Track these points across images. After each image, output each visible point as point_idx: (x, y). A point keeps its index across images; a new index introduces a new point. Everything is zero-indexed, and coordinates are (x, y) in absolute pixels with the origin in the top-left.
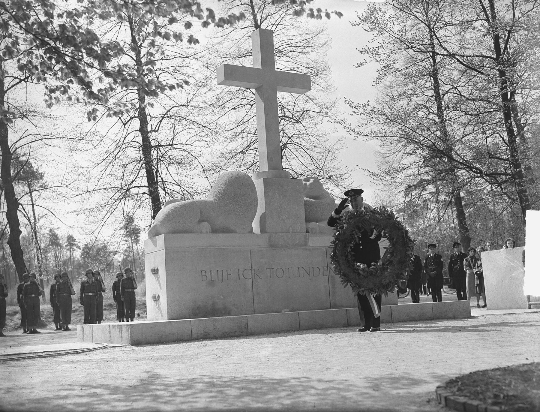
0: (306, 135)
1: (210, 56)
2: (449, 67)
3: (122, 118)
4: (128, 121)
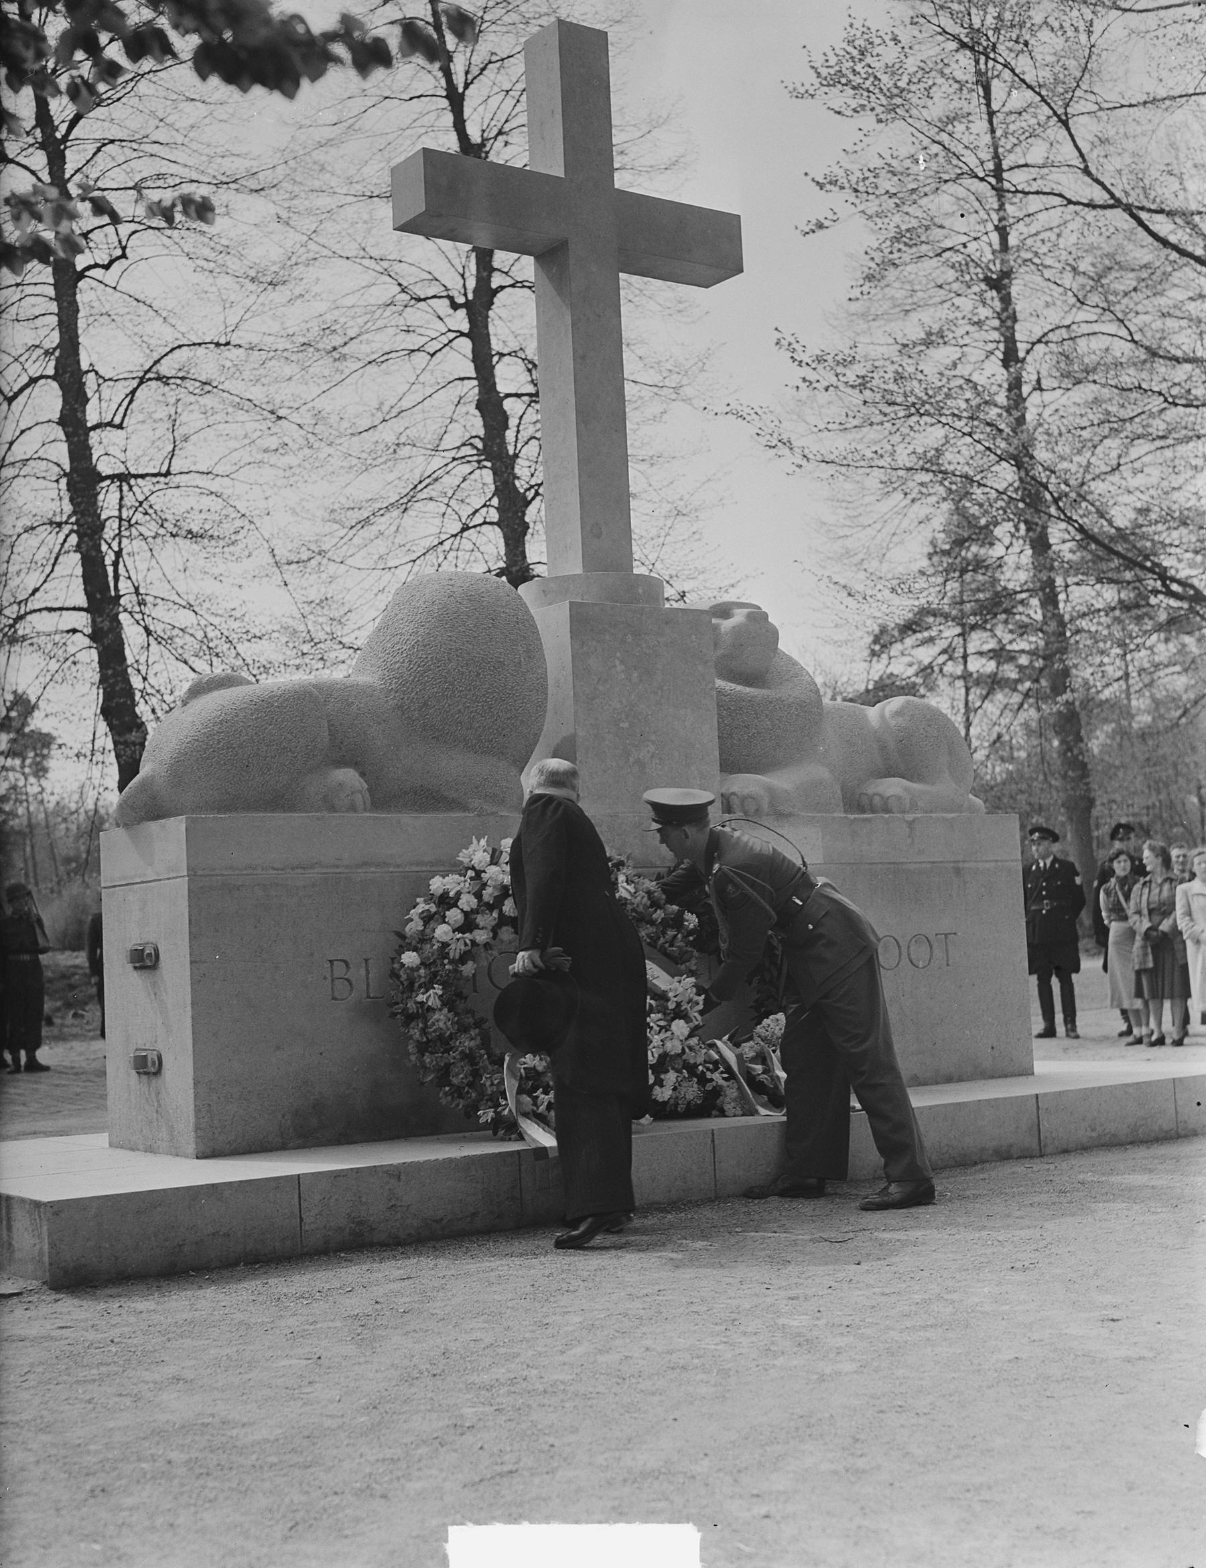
4: (22, 390)
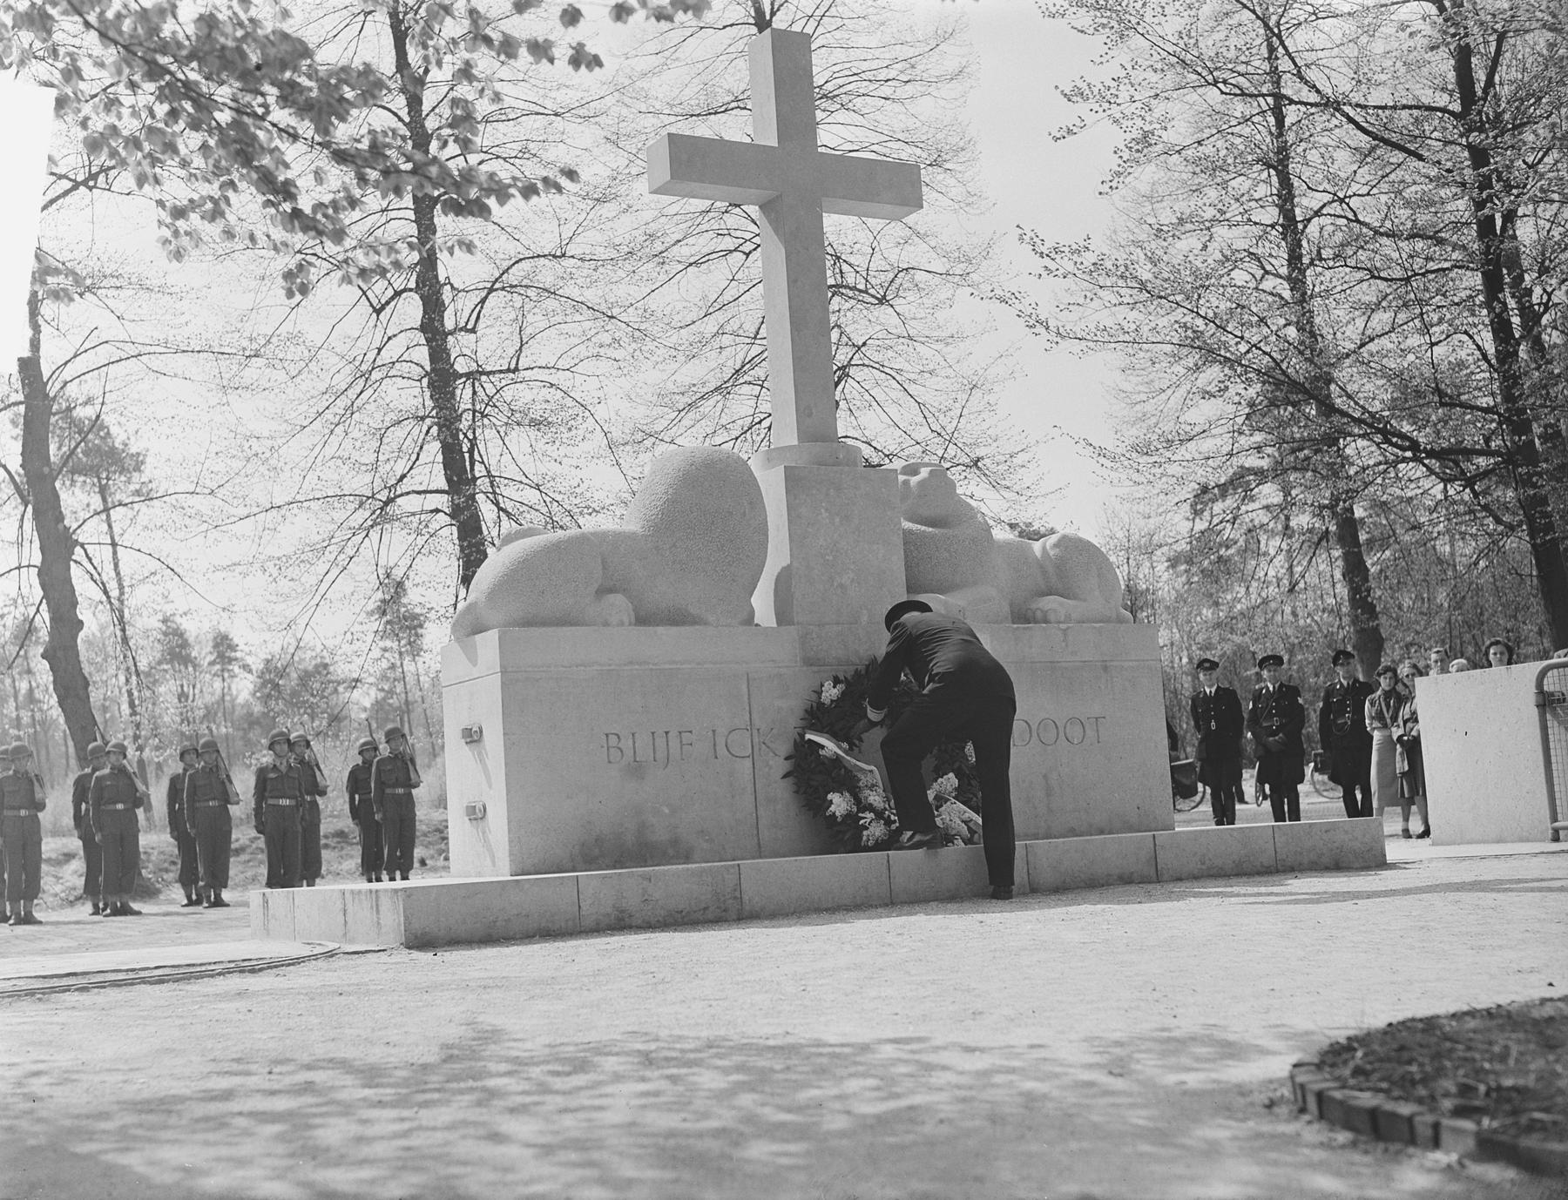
0: (906, 341)
1: (625, 111)
2: (1324, 140)
3: (369, 293)
4: (388, 303)
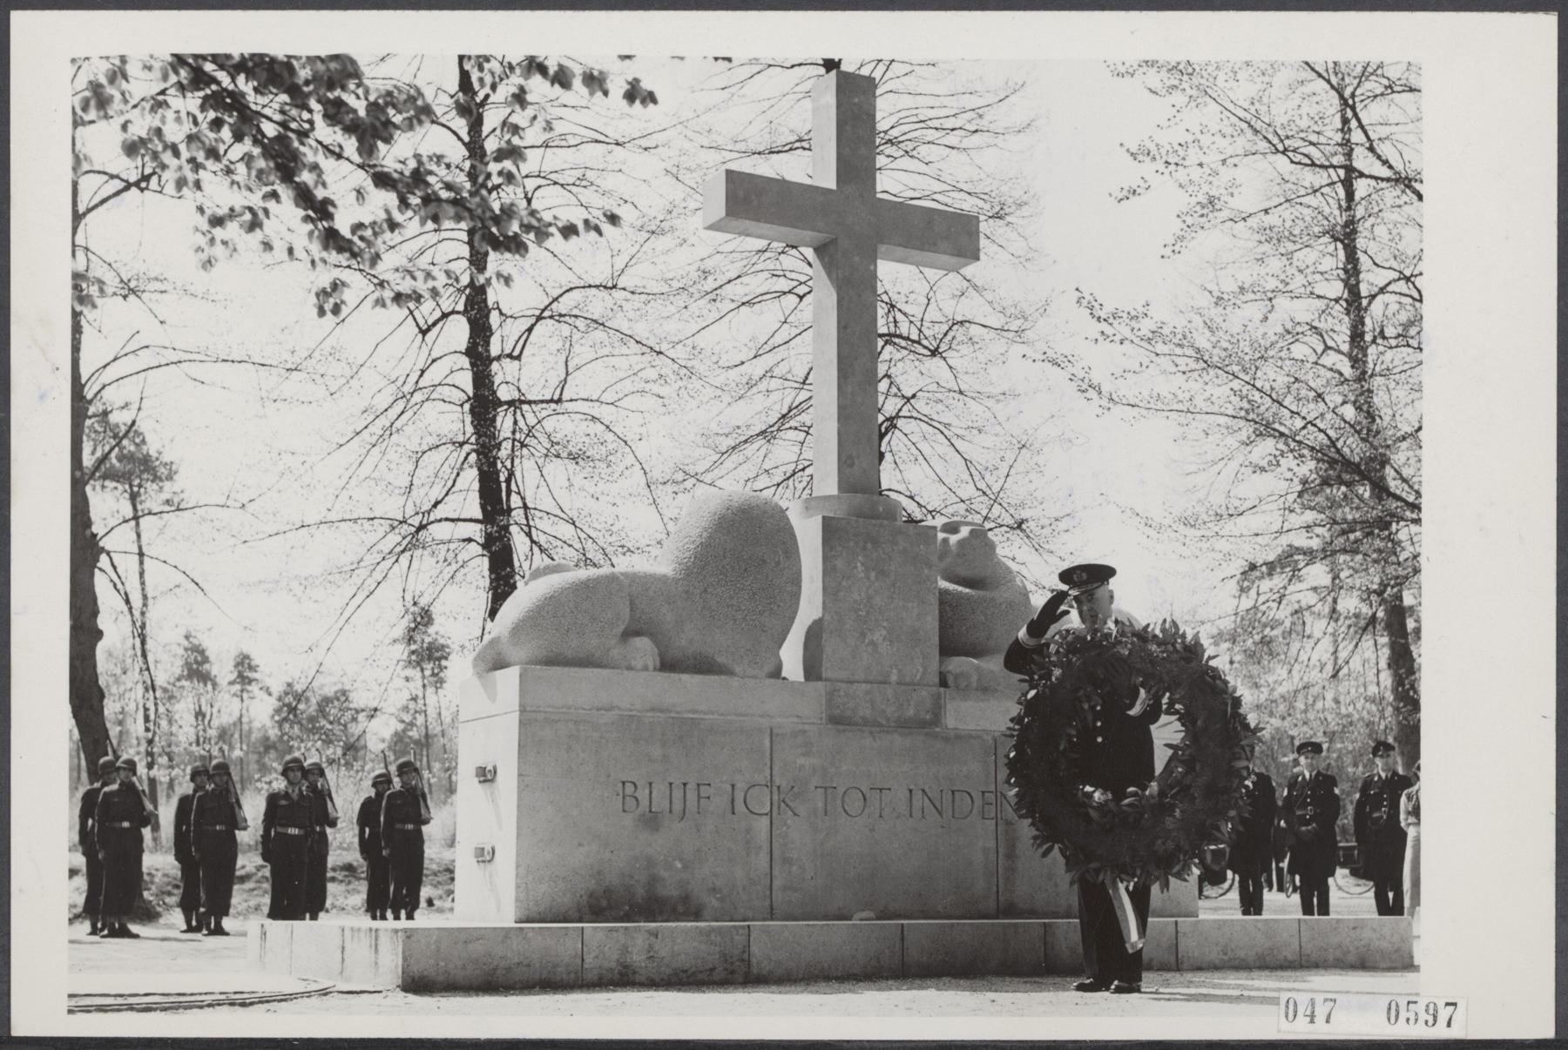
4: (434, 324)
